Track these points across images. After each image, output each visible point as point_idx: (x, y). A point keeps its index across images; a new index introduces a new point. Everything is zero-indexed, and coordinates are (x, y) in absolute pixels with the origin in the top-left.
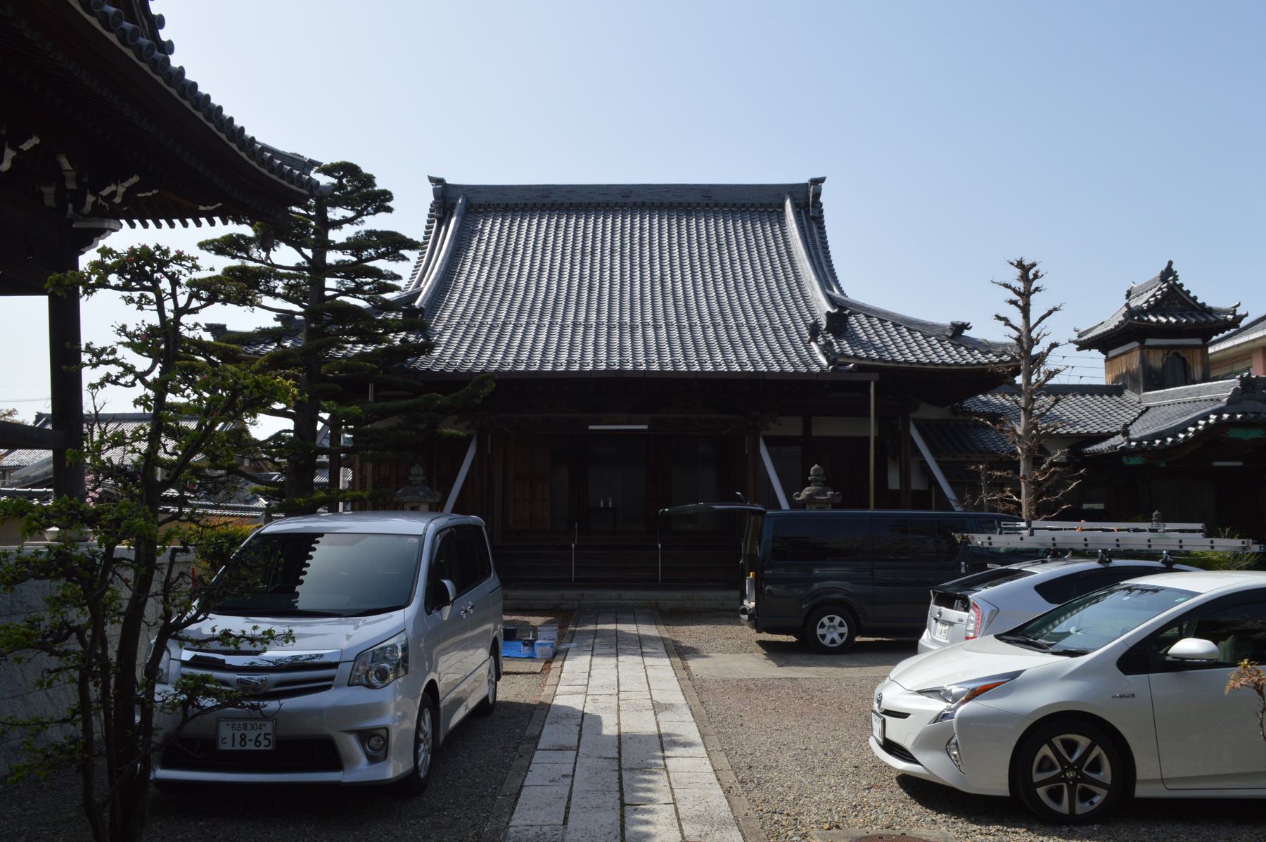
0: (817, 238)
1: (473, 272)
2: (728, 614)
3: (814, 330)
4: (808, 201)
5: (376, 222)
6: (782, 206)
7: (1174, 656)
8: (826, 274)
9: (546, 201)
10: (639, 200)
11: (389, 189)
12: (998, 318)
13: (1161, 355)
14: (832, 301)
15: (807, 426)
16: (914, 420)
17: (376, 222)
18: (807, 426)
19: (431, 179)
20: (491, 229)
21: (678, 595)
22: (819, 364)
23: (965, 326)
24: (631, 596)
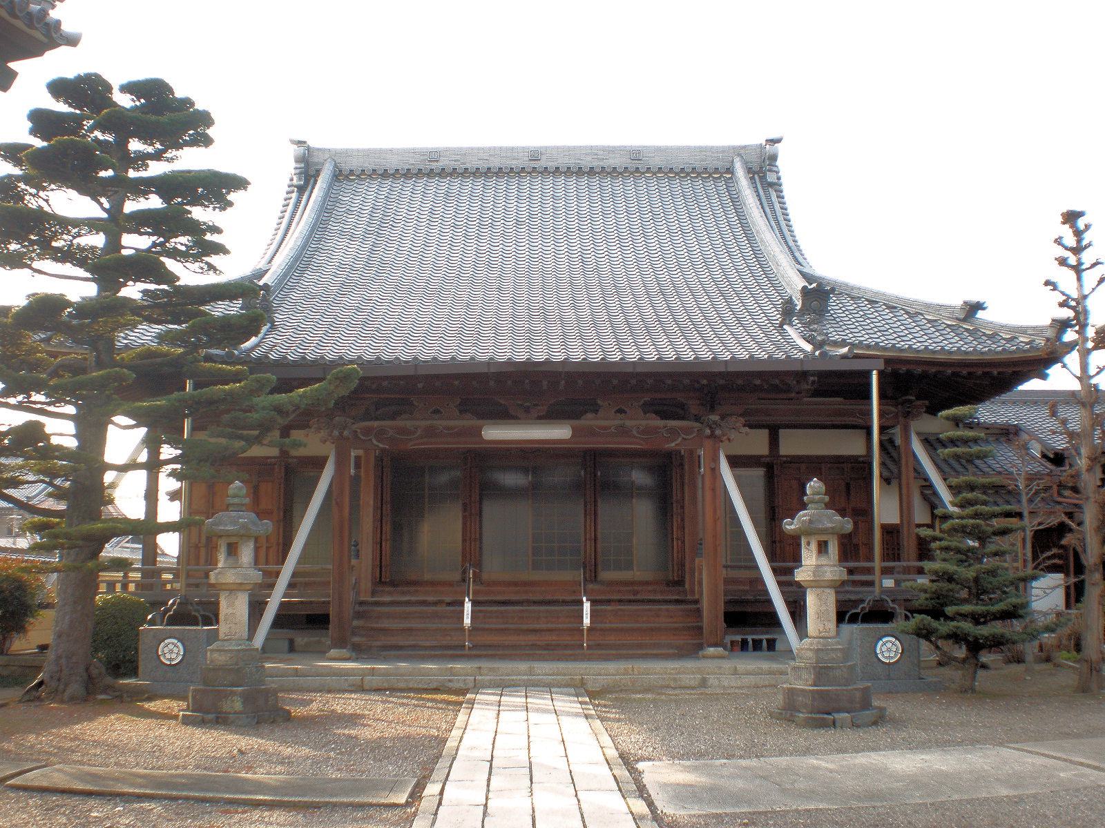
0: (777, 206)
1: (341, 252)
2: (135, 152)
3: (788, 311)
4: (763, 168)
5: (189, 159)
6: (462, 604)
7: (134, 420)
8: (794, 252)
9: (434, 165)
10: (551, 165)
11: (216, 121)
12: (1047, 283)
13: (12, 648)
14: (804, 275)
15: (774, 442)
16: (918, 434)
17: (189, 159)
18: (774, 442)
19: (293, 142)
20: (363, 198)
21: (611, 666)
22: (802, 350)
23: (977, 307)
24: (544, 668)
